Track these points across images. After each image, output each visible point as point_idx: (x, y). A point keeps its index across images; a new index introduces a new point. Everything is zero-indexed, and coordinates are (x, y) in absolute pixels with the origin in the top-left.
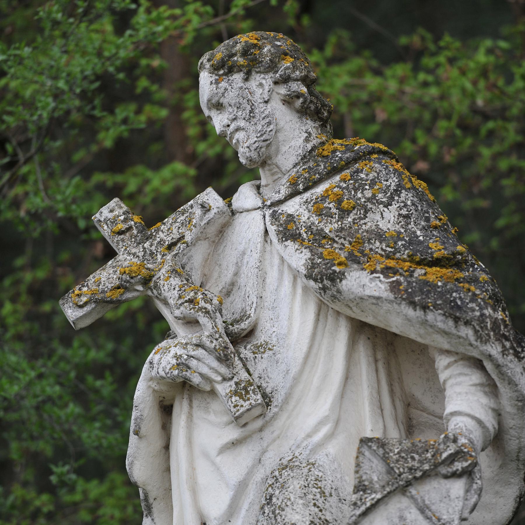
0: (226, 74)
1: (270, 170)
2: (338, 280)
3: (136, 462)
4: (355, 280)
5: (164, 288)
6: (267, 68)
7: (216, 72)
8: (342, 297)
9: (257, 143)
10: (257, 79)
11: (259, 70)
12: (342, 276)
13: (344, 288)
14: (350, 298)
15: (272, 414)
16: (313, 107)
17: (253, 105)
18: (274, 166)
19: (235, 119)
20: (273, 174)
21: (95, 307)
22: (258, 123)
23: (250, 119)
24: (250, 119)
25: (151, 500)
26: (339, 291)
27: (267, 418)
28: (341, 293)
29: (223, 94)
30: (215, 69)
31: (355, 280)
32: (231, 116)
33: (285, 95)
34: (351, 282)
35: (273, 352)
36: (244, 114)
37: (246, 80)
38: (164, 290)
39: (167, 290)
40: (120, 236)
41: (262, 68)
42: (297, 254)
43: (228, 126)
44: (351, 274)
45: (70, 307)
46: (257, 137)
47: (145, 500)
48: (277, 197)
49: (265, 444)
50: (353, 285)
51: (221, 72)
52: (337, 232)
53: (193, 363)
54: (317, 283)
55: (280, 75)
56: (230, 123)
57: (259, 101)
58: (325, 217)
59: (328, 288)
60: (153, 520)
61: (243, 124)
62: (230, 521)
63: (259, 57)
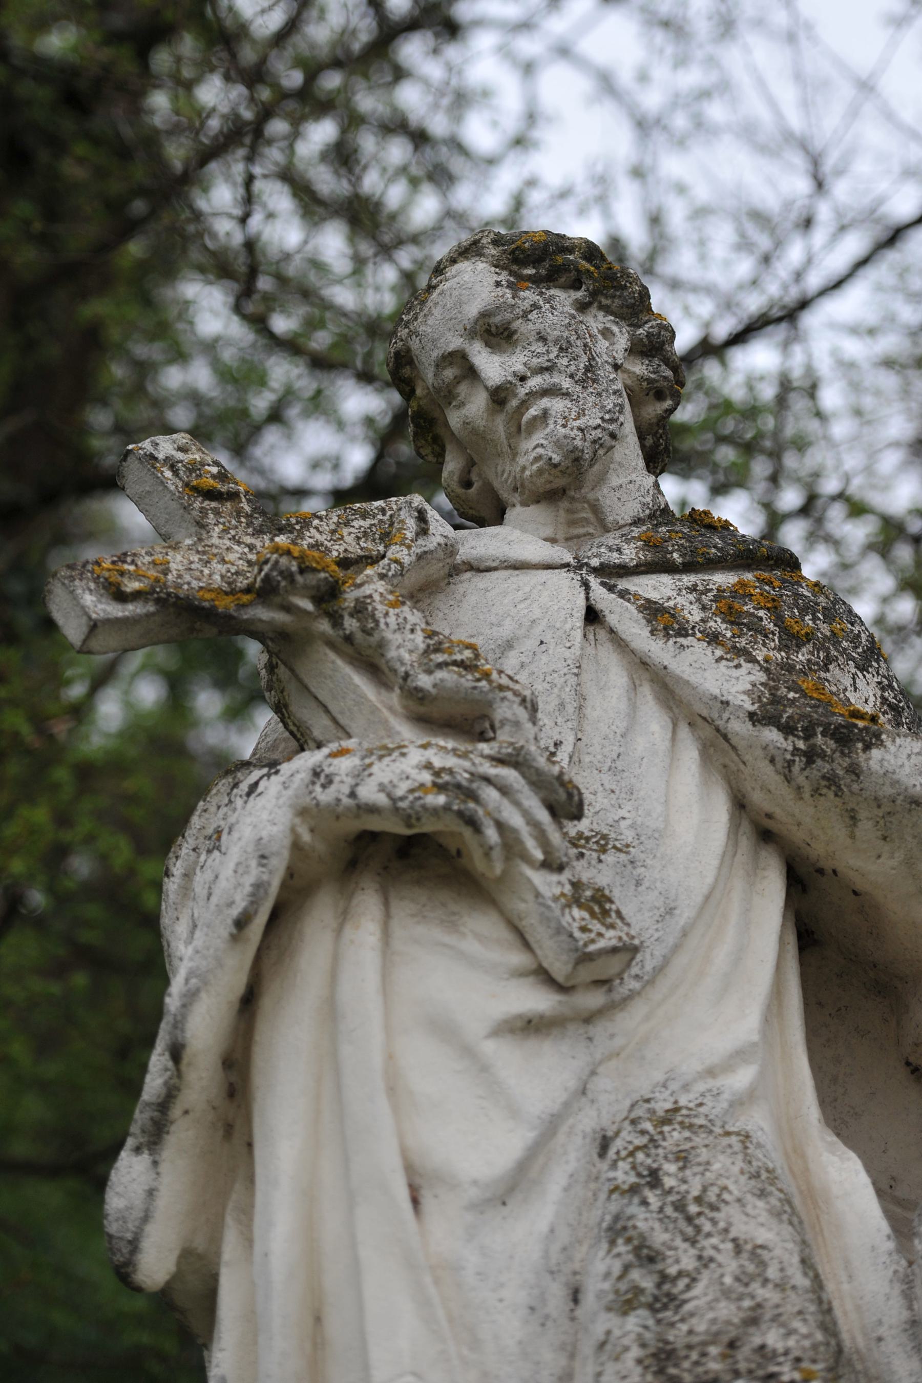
0: (536, 281)
1: (569, 511)
2: (860, 745)
3: (203, 995)
4: (909, 756)
5: (388, 620)
6: (627, 307)
7: (515, 268)
8: (855, 787)
9: (600, 430)
10: (596, 321)
11: (609, 302)
12: (872, 740)
13: (874, 765)
14: (881, 793)
15: (627, 992)
16: (651, 441)
17: (594, 359)
18: (586, 505)
19: (547, 369)
20: (572, 523)
21: (153, 614)
22: (604, 394)
23: (584, 381)
24: (584, 381)
25: (176, 1112)
26: (854, 771)
27: (616, 996)
28: (858, 776)
29: (525, 315)
30: (516, 261)
31: (909, 756)
32: (542, 361)
33: (642, 379)
34: (896, 756)
35: (629, 857)
36: (573, 368)
37: (582, 307)
38: (387, 624)
39: (393, 626)
40: (207, 502)
41: (617, 302)
42: (724, 670)
43: (523, 379)
44: (898, 740)
45: (90, 590)
46: (602, 418)
47: (159, 1105)
48: (615, 558)
49: (598, 1056)
50: (902, 766)
51: (530, 271)
52: (782, 669)
53: (491, 794)
54: (791, 738)
55: (648, 332)
56: (529, 374)
57: (605, 358)
58: (750, 630)
59: (823, 755)
60: (155, 1163)
61: (568, 386)
62: (504, 1204)
63: (622, 277)
